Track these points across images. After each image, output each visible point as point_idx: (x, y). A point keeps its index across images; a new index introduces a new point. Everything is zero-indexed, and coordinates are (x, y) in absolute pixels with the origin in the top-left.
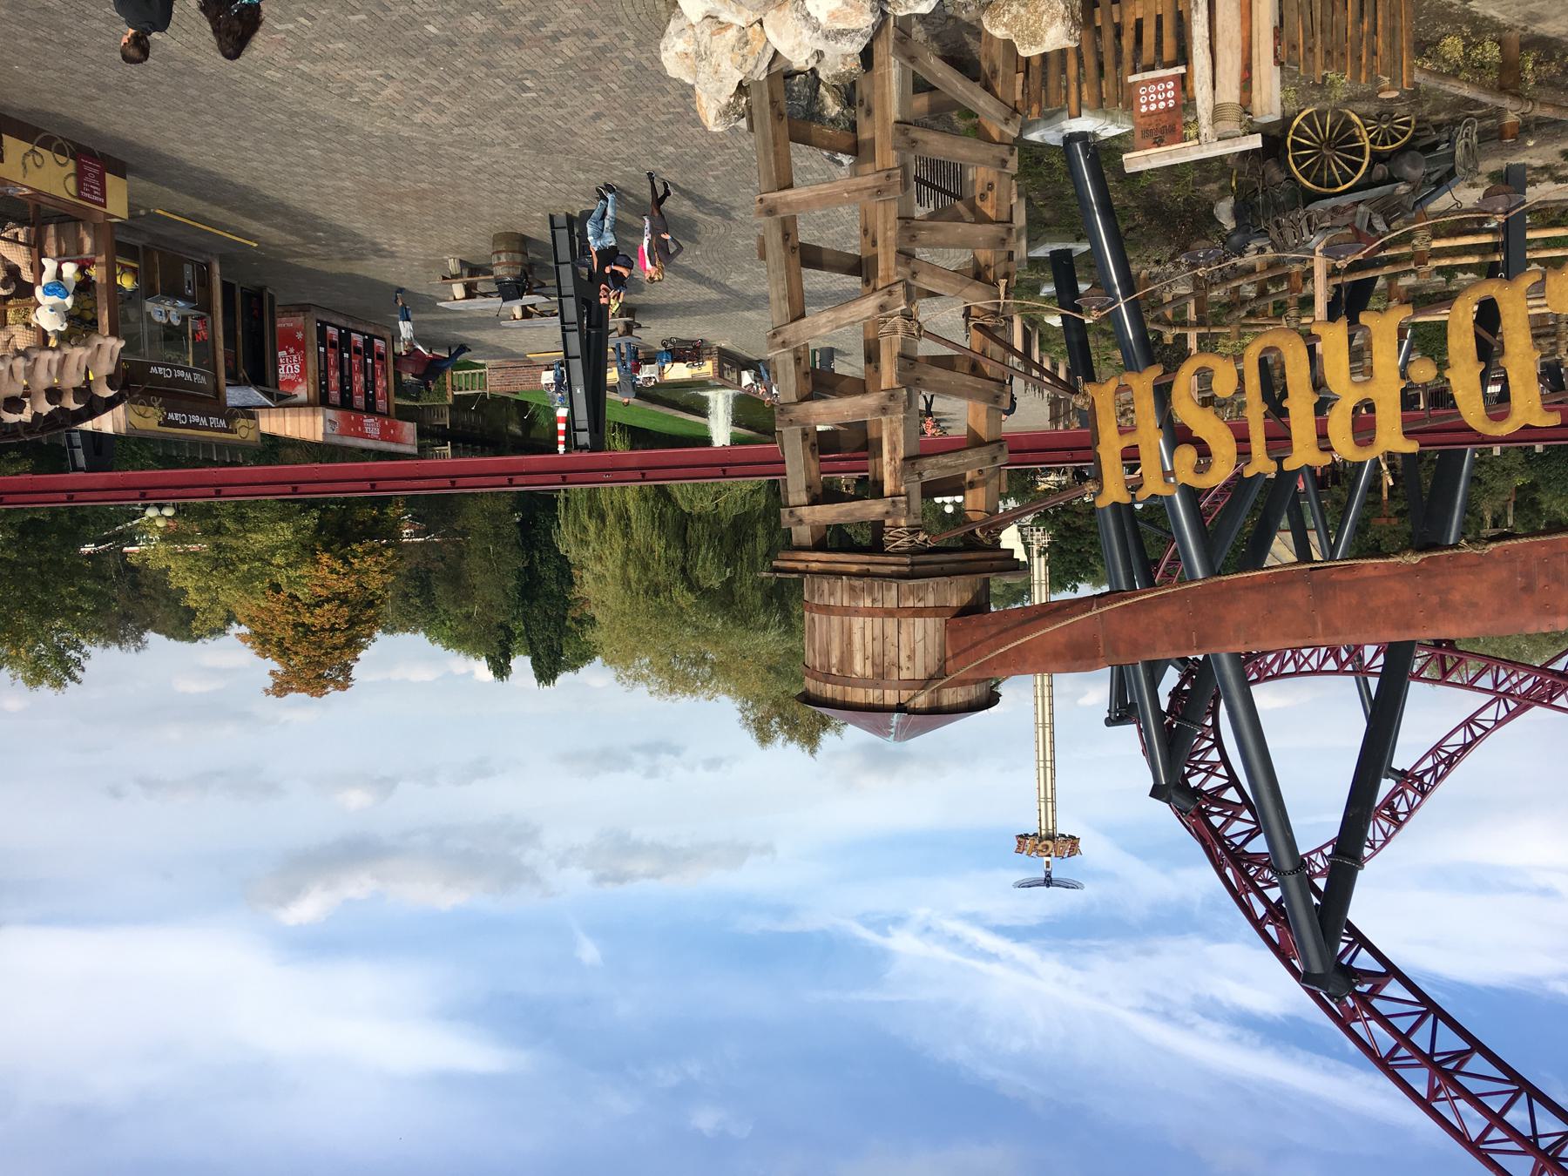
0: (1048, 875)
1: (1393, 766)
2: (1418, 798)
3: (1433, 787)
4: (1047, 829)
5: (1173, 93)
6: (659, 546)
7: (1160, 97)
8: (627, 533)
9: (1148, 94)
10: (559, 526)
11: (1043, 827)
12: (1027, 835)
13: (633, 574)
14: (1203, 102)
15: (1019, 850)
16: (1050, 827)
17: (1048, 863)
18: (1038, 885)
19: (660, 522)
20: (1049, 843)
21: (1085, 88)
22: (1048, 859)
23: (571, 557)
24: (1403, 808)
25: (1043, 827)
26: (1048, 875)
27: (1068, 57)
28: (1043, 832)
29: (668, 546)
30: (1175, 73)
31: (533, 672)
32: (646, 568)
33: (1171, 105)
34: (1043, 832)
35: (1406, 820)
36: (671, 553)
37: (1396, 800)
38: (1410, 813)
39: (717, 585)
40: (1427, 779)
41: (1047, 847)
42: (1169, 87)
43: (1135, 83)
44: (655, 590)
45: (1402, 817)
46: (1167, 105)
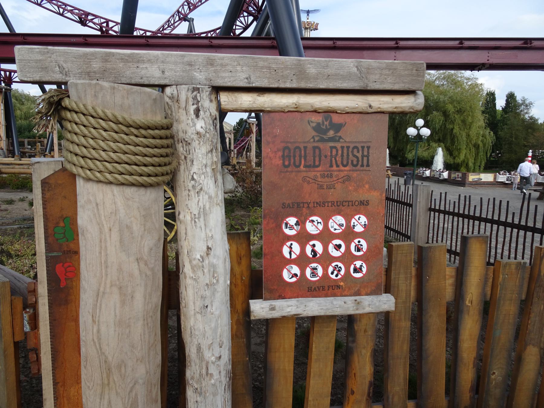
0: (308, 15)
1: (188, 23)
2: (180, 10)
3: (175, 14)
4: (307, 32)
5: (286, 251)
6: (456, 130)
7: (319, 248)
8: (468, 136)
9: (347, 258)
10: (492, 142)
11: (309, 33)
12: (314, 30)
13: (470, 119)
14: (204, 213)
15: (317, 24)
16: (306, 33)
17: (308, 19)
18: (312, 11)
19: (453, 138)
20: (307, 27)
21: (449, 293)
22: (308, 21)
23: (488, 130)
24: (186, 8)
25: (309, 33)
26: (308, 15)
27: (473, 355)
28: (309, 31)
29: (452, 129)
30: (278, 303)
31: (496, 96)
32: (464, 121)
33: (292, 221)
34: (309, 31)
35: (184, 2)
36: (451, 126)
37: (188, 11)
38: (183, 5)
39: (435, 112)
40: (177, 19)
41: (308, 25)
42: (296, 270)
43: (376, 292)
44: (460, 111)
45: (186, 3)
46: (301, 223)
